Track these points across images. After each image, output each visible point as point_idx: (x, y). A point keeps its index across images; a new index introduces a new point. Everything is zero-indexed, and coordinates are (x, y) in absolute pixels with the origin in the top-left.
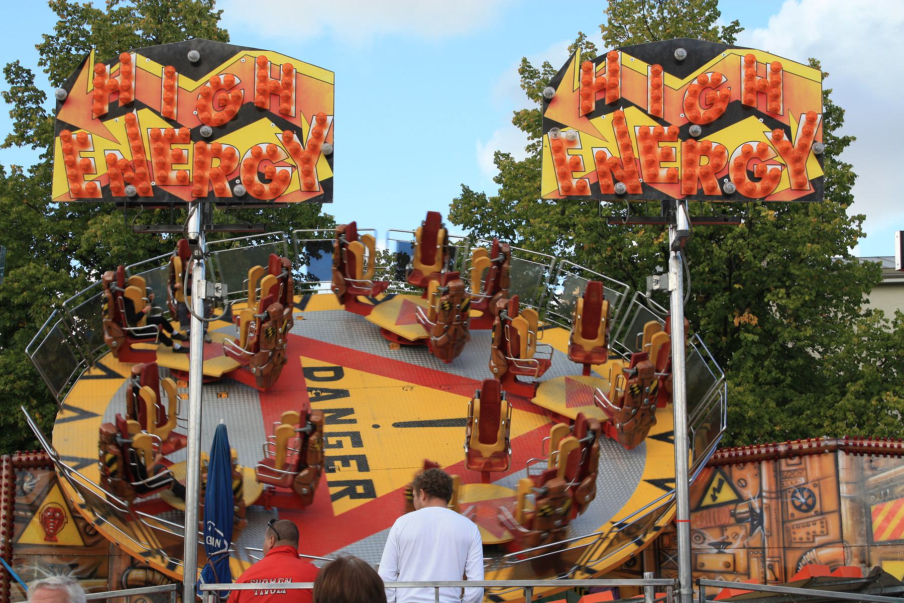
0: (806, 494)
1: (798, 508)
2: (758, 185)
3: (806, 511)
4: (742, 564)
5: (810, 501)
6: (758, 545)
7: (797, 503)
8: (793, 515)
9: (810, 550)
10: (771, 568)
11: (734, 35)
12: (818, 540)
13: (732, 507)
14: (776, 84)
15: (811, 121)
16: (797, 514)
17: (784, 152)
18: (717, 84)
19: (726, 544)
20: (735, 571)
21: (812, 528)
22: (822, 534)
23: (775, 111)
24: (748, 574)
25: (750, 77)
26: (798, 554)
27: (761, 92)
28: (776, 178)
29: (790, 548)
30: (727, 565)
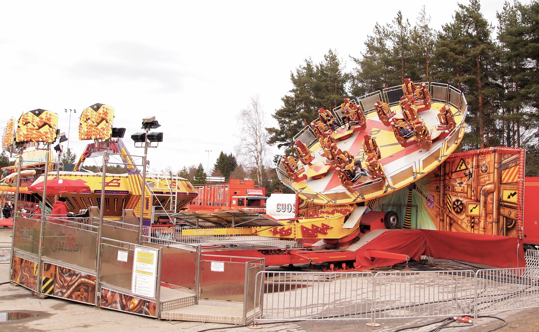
4: (466, 190)
12: (487, 182)
13: (464, 171)
16: (482, 173)
24: (467, 193)
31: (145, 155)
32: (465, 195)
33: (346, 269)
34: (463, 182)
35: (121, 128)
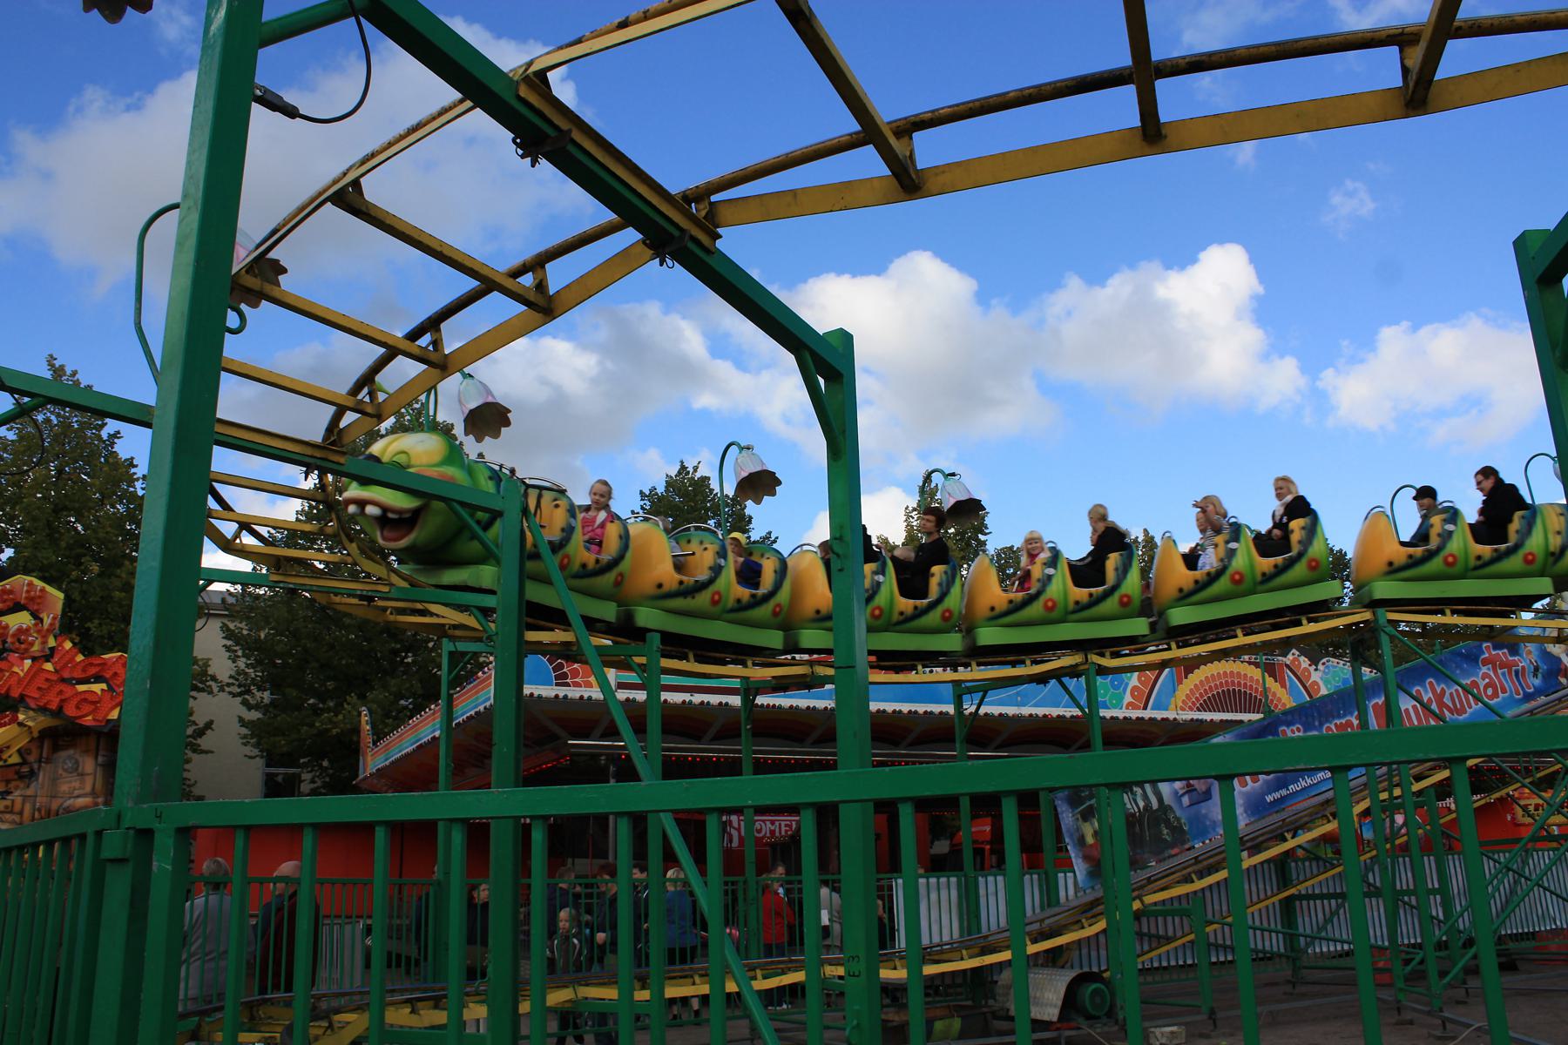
0: (73, 761)
1: (66, 770)
2: (23, 646)
3: (71, 773)
4: (18, 807)
5: (75, 766)
6: (32, 794)
7: (66, 767)
8: (61, 775)
9: (70, 798)
10: (39, 810)
11: (116, 440)
12: (76, 793)
13: (17, 767)
14: (40, 597)
15: (54, 618)
16: (64, 774)
17: (39, 631)
18: (11, 592)
19: (9, 793)
20: (11, 812)
21: (73, 784)
22: (80, 788)
23: (37, 611)
24: (21, 813)
25: (28, 592)
26: (61, 801)
27: (32, 599)
28: (32, 644)
29: (55, 797)
30: (7, 807)
31: (308, 840)
32: (17, 818)
33: (548, 885)
34: (12, 790)
35: (1309, 500)
